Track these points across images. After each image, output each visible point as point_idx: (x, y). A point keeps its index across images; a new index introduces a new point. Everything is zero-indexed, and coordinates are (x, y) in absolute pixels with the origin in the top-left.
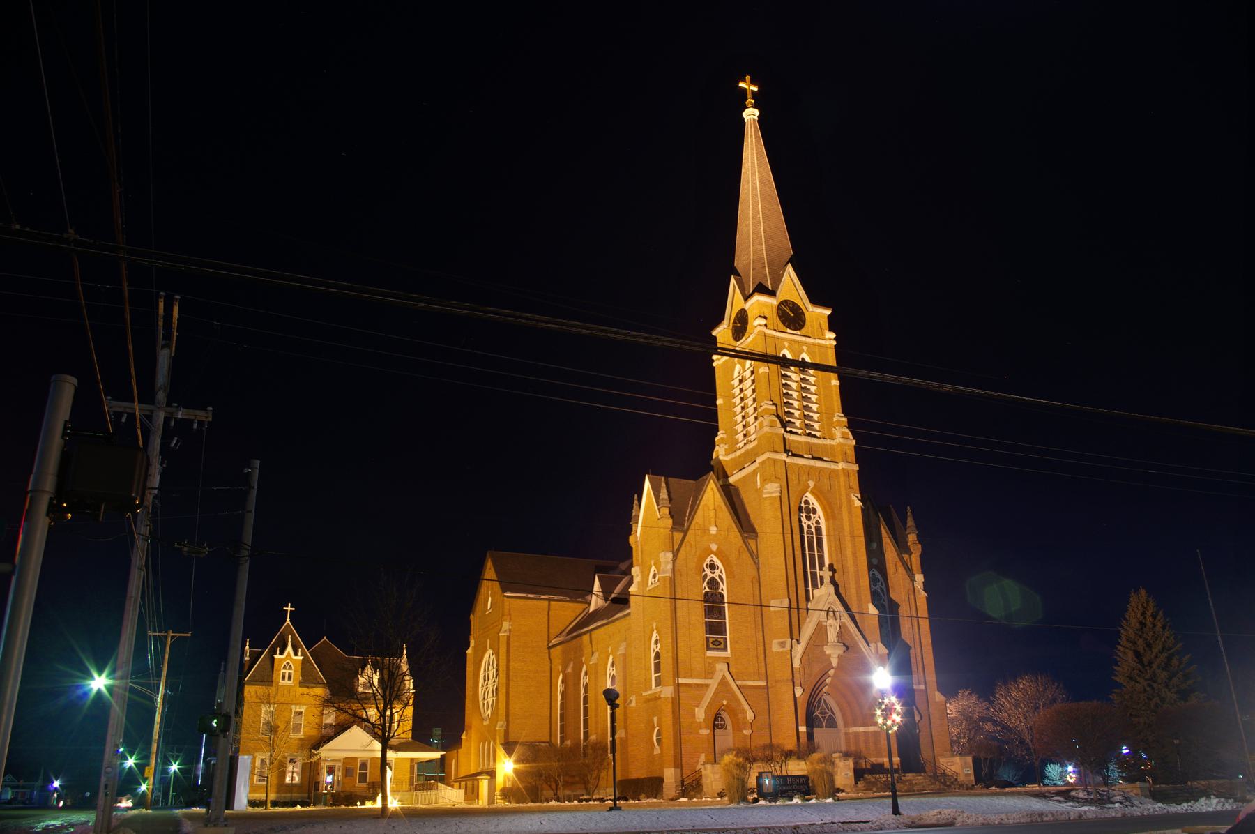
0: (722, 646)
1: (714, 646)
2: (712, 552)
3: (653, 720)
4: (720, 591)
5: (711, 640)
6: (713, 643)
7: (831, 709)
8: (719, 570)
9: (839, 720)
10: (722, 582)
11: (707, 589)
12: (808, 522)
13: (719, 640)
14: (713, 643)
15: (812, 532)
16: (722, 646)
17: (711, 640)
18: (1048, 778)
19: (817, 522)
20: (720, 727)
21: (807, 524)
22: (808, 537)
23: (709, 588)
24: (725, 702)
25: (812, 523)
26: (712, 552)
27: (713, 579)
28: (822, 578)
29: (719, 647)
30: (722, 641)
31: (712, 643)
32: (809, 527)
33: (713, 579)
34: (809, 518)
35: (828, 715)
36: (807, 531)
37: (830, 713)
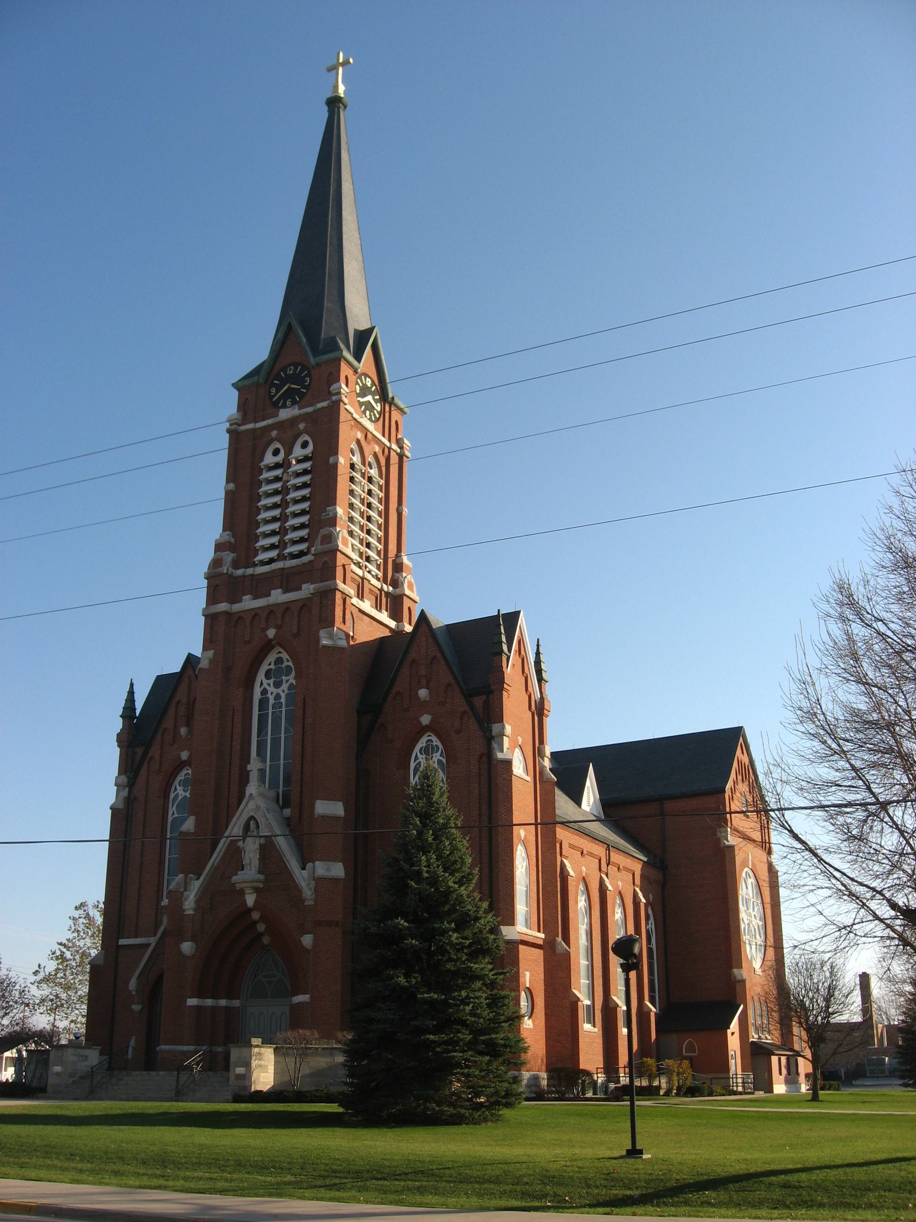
12: (275, 691)
21: (274, 695)
32: (278, 697)
34: (278, 685)
36: (273, 705)
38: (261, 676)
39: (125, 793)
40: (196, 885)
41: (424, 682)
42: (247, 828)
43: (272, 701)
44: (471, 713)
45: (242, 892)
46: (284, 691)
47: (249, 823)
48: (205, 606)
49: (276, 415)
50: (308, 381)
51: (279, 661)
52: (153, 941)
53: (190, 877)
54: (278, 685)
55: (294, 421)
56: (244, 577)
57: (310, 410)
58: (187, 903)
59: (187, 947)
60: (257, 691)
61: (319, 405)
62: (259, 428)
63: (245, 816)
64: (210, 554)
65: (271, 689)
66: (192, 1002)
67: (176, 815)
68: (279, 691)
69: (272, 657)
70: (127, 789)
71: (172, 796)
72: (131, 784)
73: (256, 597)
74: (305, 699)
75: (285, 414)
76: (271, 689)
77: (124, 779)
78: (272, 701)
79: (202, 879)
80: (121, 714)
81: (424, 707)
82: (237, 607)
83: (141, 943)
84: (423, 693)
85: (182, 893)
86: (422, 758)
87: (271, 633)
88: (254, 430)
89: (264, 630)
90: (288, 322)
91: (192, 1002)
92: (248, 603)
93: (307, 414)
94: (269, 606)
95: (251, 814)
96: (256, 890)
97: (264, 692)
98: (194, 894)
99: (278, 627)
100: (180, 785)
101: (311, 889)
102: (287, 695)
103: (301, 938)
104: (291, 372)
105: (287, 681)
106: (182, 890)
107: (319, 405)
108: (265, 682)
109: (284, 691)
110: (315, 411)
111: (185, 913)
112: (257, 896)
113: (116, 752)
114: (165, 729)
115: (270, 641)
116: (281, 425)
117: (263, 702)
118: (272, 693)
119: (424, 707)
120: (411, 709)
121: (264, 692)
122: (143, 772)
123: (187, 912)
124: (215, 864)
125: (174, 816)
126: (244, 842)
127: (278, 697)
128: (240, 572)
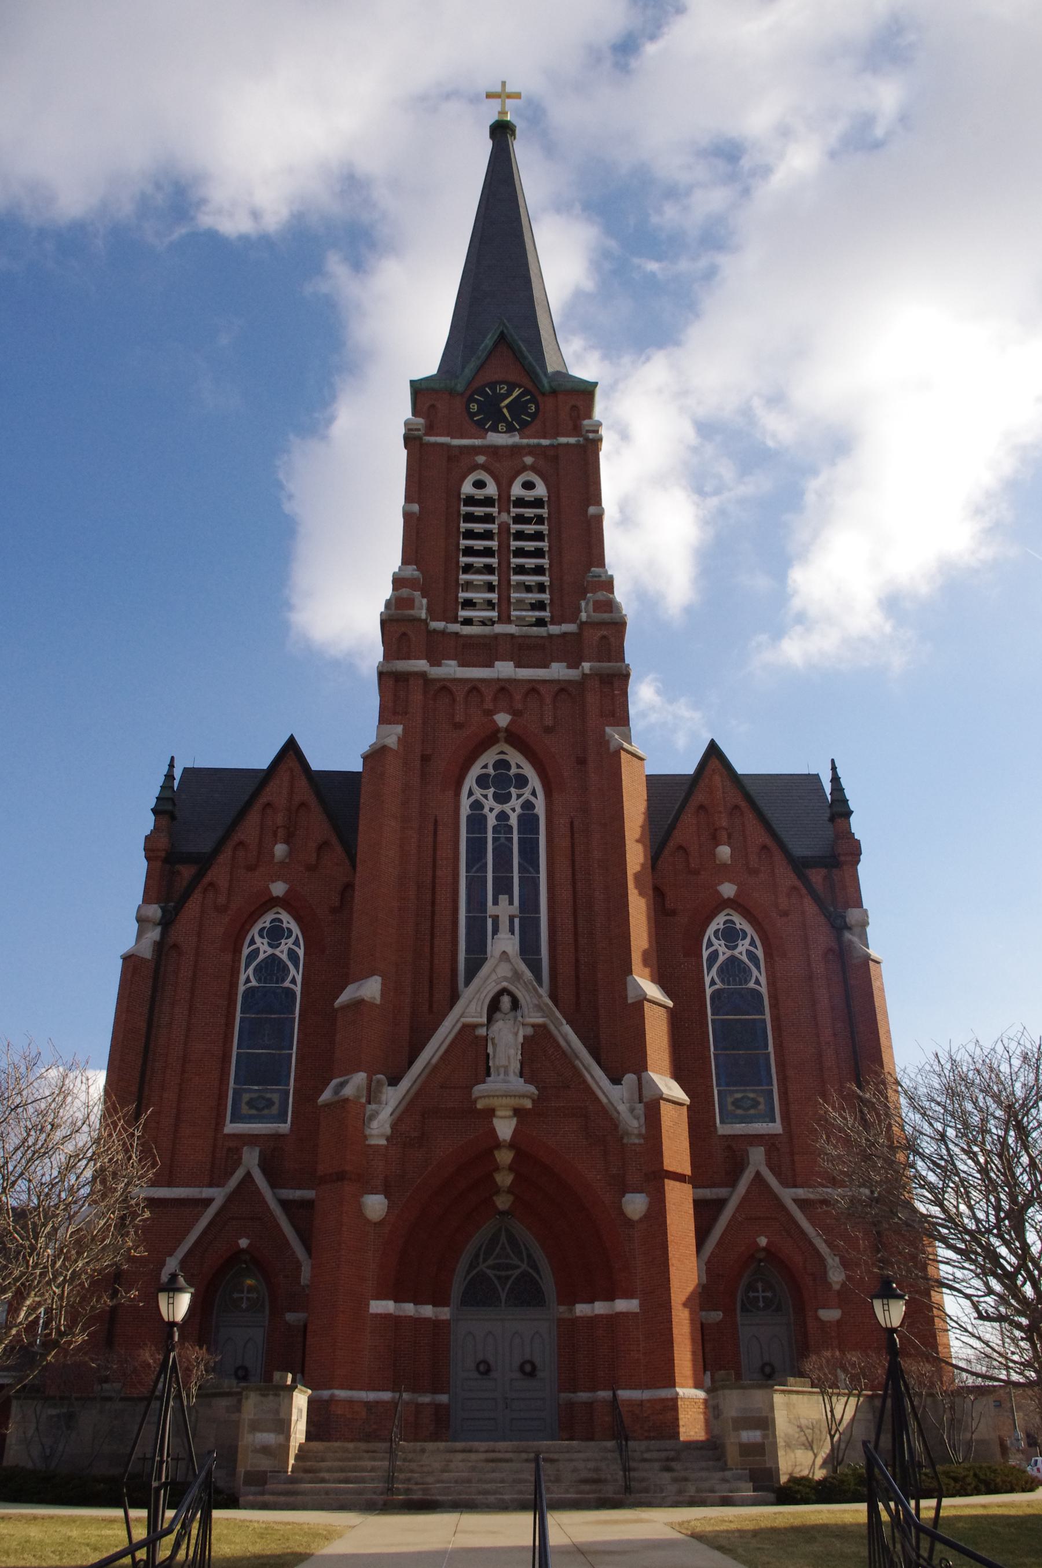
0: (275, 1110)
1: (253, 1112)
2: (273, 902)
3: (628, 1295)
4: (287, 984)
5: (246, 1097)
6: (250, 1104)
7: (529, 1256)
8: (748, 940)
9: (548, 1283)
10: (758, 968)
11: (254, 983)
12: (498, 808)
13: (268, 1096)
14: (250, 1104)
15: (511, 828)
16: (275, 1110)
17: (246, 1097)
18: (808, 1475)
19: (528, 806)
20: (761, 1304)
21: (495, 812)
22: (495, 839)
23: (723, 981)
24: (763, 1241)
25: (514, 809)
26: (273, 902)
27: (733, 960)
28: (496, 919)
29: (266, 1112)
30: (276, 1097)
31: (248, 1103)
32: (503, 816)
33: (733, 960)
34: (502, 798)
35: (517, 1272)
36: (494, 827)
37: (524, 1266)
38: (470, 781)
39: (154, 934)
40: (392, 1098)
41: (724, 835)
42: (494, 1007)
43: (491, 821)
44: (804, 891)
45: (490, 1113)
46: (514, 810)
47: (499, 1002)
48: (382, 660)
49: (484, 438)
50: (533, 408)
51: (502, 765)
52: (218, 1195)
53: (379, 1081)
54: (502, 798)
55: (515, 451)
56: (443, 633)
57: (545, 442)
58: (375, 1124)
59: (375, 1205)
60: (465, 804)
61: (563, 440)
62: (455, 447)
63: (491, 989)
64: (387, 591)
65: (489, 803)
66: (381, 1306)
67: (719, 985)
68: (506, 807)
69: (489, 757)
70: (158, 930)
71: (246, 951)
72: (166, 923)
73: (462, 664)
74: (572, 823)
75: (498, 439)
76: (489, 803)
77: (155, 911)
78: (491, 821)
79: (405, 1084)
80: (153, 807)
81: (724, 872)
82: (436, 672)
83: (182, 1196)
84: (724, 852)
85: (363, 1106)
86: (719, 945)
87: (503, 720)
88: (448, 447)
89: (490, 713)
90: (499, 332)
91: (381, 1306)
92: (451, 669)
93: (539, 446)
94: (499, 680)
95: (505, 984)
96: (518, 1112)
97: (477, 805)
98: (389, 1110)
99: (515, 713)
100: (262, 936)
101: (637, 1118)
102: (520, 817)
103: (167, 1258)
104: (502, 391)
105: (486, 797)
106: (363, 1100)
107: (563, 440)
108: (478, 792)
109: (514, 810)
110: (552, 446)
111: (367, 1143)
112: (518, 1122)
113: (141, 866)
114: (241, 843)
115: (498, 730)
116: (494, 451)
117: (477, 821)
118: (491, 810)
119: (724, 872)
120: (703, 873)
121: (477, 805)
122: (193, 906)
123: (373, 1142)
124: (434, 1061)
125: (250, 985)
126: (487, 1030)
127: (503, 816)
128: (438, 625)
